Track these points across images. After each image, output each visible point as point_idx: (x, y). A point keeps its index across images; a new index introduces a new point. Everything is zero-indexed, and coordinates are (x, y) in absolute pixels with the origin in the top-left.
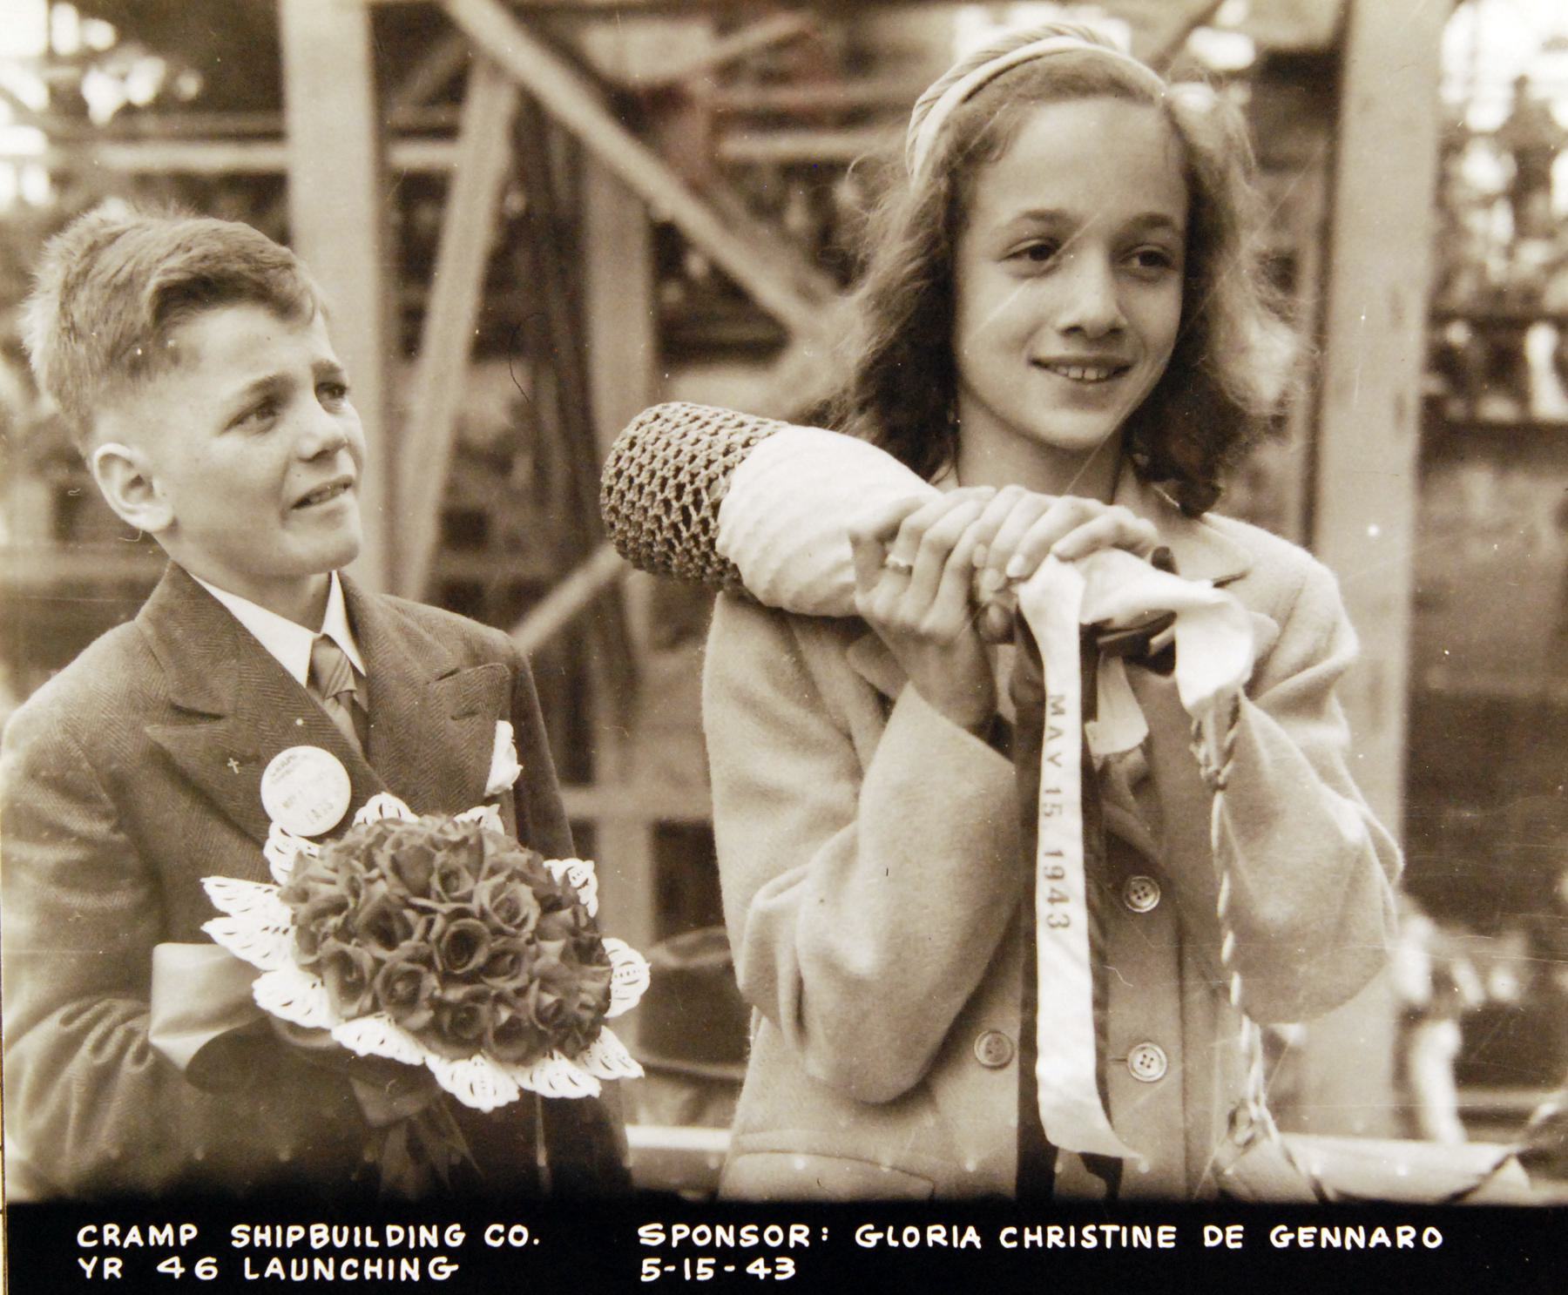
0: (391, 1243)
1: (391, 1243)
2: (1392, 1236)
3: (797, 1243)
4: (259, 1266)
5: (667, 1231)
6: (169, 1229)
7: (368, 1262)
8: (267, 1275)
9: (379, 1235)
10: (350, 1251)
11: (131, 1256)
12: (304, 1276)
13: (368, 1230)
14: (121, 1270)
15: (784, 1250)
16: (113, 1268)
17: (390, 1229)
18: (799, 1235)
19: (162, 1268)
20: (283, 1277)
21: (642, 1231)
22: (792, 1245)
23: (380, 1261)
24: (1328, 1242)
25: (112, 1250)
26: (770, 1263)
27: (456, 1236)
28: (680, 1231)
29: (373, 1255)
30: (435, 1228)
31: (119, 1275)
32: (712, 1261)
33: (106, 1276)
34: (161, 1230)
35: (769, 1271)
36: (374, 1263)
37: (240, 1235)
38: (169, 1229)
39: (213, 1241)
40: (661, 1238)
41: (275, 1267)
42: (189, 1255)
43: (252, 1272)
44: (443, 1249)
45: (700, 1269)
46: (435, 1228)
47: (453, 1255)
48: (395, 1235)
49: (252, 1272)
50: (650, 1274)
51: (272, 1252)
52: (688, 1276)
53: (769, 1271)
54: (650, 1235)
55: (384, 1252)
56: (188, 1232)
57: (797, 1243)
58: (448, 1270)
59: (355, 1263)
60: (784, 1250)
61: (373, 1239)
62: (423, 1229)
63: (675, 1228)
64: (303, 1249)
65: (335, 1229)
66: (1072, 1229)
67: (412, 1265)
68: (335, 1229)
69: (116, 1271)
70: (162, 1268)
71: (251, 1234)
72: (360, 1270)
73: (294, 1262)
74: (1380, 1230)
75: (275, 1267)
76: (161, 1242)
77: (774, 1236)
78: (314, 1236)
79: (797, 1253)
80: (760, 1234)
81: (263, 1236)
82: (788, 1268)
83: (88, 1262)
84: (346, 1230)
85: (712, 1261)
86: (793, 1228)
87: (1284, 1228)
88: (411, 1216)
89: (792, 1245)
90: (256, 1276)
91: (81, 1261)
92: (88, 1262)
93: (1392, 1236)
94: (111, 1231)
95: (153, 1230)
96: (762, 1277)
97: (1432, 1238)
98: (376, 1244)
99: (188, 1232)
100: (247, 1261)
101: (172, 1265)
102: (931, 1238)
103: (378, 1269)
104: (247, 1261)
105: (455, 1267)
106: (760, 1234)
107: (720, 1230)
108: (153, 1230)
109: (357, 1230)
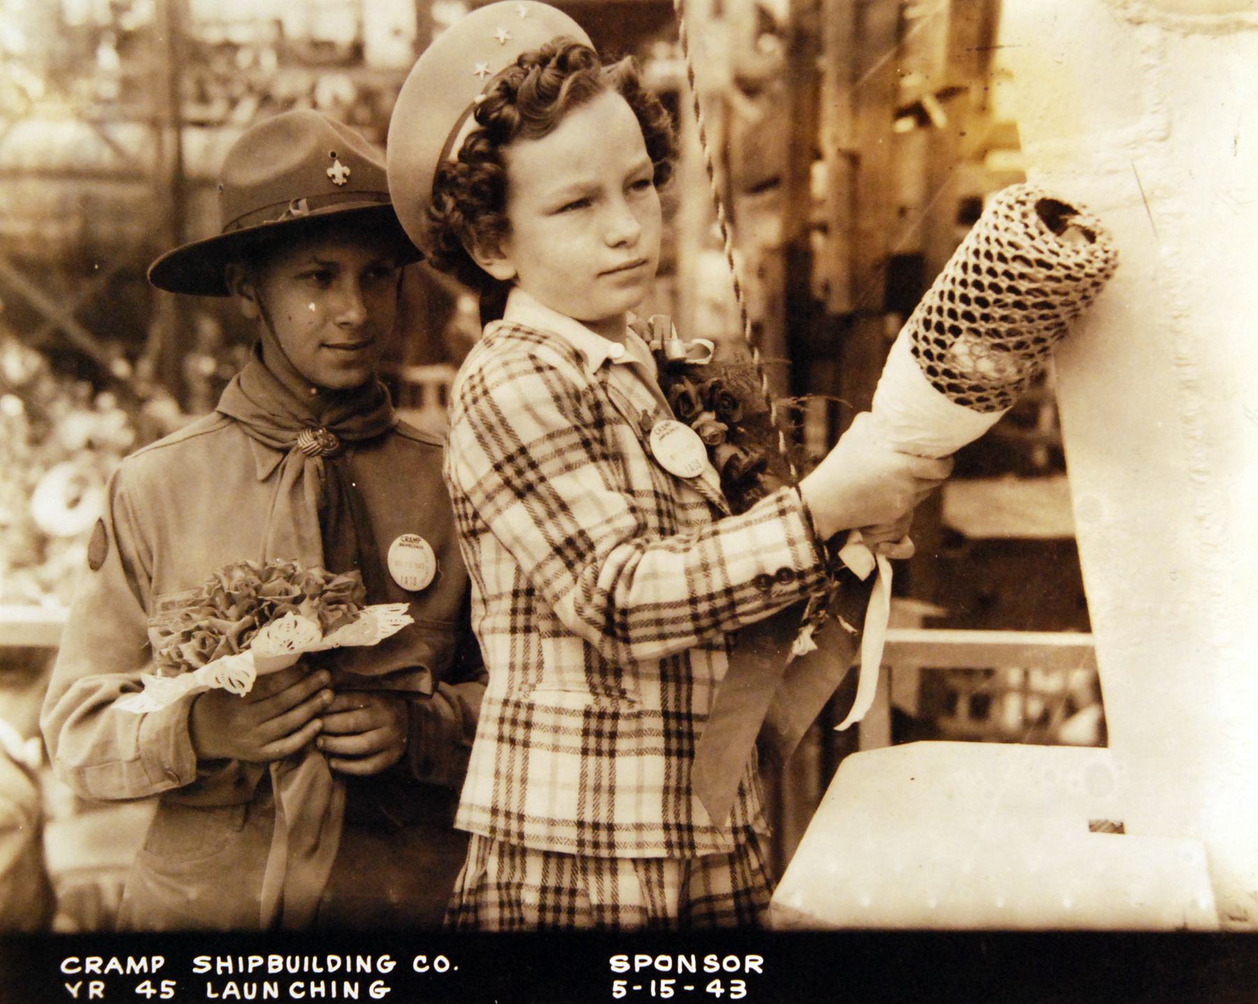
0: (331, 969)
1: (331, 969)
2: (124, 964)
3: (751, 970)
4: (219, 988)
5: (631, 962)
6: (144, 960)
7: (312, 984)
8: (224, 996)
9: (322, 963)
10: (301, 976)
11: (111, 979)
12: (253, 996)
13: (315, 959)
14: (103, 992)
15: (740, 974)
16: (96, 989)
17: (330, 958)
18: (754, 963)
19: (139, 990)
20: (238, 997)
21: (613, 960)
22: (747, 971)
23: (322, 983)
24: (362, 968)
25: (93, 976)
26: (156, 985)
27: (387, 965)
28: (255, 961)
29: (317, 978)
30: (369, 958)
31: (101, 996)
32: (673, 981)
33: (91, 996)
34: (137, 962)
35: (154, 991)
36: (318, 985)
37: (202, 963)
38: (144, 960)
39: (178, 968)
40: (208, 967)
41: (231, 989)
42: (156, 980)
43: (213, 992)
44: (375, 975)
45: (663, 988)
46: (369, 958)
47: (388, 979)
48: (334, 963)
49: (213, 992)
50: (619, 992)
51: (226, 978)
52: (653, 994)
53: (154, 991)
54: (618, 963)
55: (327, 977)
56: (158, 962)
57: (751, 970)
58: (384, 991)
59: (301, 985)
60: (740, 974)
61: (319, 966)
62: (359, 959)
63: (638, 957)
64: (261, 975)
65: (289, 958)
66: (348, 958)
67: (353, 987)
68: (289, 958)
69: (99, 993)
70: (139, 990)
71: (213, 963)
72: (307, 989)
73: (246, 985)
74: (114, 960)
75: (231, 989)
76: (137, 972)
77: (731, 964)
78: (271, 964)
79: (750, 978)
80: (720, 961)
81: (225, 964)
82: (740, 989)
83: (73, 986)
84: (297, 958)
85: (625, 983)
86: (748, 958)
87: (387, 957)
88: (349, 948)
89: (747, 971)
90: (216, 995)
91: (68, 986)
92: (73, 986)
93: (124, 964)
94: (158, 962)
95: (131, 961)
96: (718, 995)
97: (441, 964)
98: (321, 970)
99: (158, 962)
100: (209, 985)
101: (145, 988)
102: (749, 965)
103: (322, 989)
104: (209, 985)
105: (388, 990)
106: (430, 962)
107: (682, 959)
108: (131, 961)
109: (348, 958)
